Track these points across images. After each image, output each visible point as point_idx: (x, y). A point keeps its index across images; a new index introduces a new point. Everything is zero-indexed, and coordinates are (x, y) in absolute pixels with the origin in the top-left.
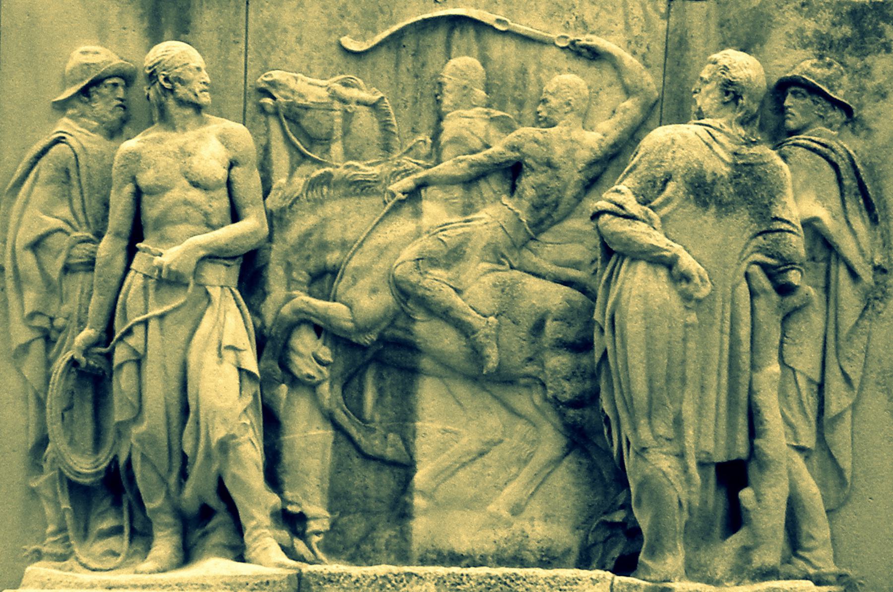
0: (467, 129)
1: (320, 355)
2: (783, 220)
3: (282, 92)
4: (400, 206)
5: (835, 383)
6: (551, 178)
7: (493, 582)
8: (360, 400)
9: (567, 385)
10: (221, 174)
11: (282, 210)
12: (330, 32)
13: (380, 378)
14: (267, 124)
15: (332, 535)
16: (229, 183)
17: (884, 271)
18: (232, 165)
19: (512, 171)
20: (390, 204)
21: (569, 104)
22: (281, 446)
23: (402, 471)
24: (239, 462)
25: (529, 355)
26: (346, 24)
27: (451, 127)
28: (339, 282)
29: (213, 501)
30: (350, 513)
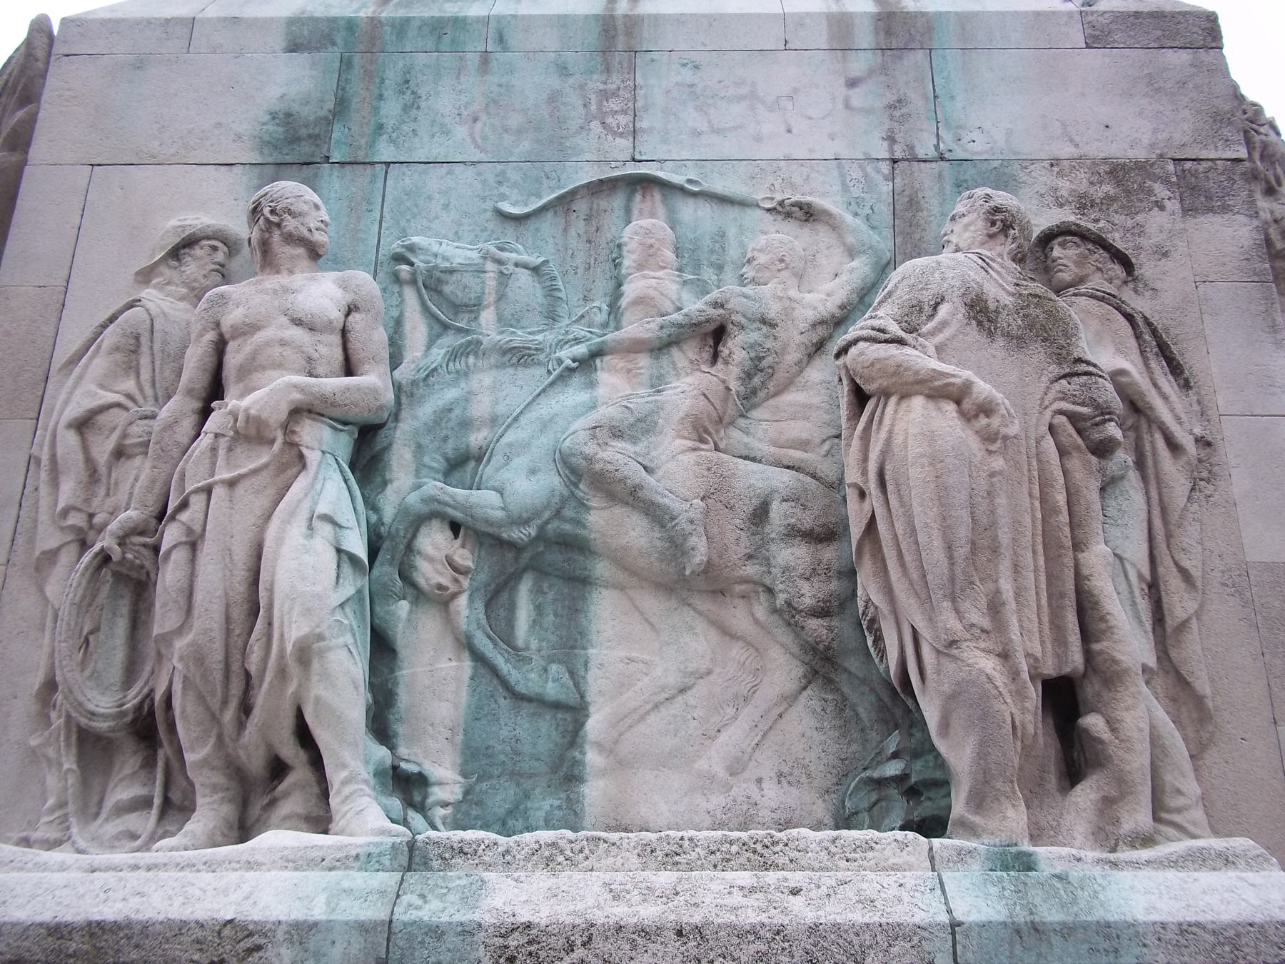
0: (655, 289)
1: (457, 558)
2: (1088, 363)
3: (422, 257)
4: (569, 376)
5: (1172, 583)
6: (767, 337)
7: (735, 848)
8: (511, 621)
9: (806, 588)
10: (336, 315)
11: (414, 383)
12: (484, 199)
13: (538, 591)
14: (401, 294)
15: (464, 807)
16: (344, 332)
17: (1209, 444)
18: (350, 310)
19: (715, 335)
20: (555, 373)
21: (782, 261)
22: (396, 683)
23: (568, 717)
24: (326, 676)
25: (748, 551)
26: (504, 189)
27: (631, 290)
28: (485, 466)
29: (290, 751)
30: (491, 777)
